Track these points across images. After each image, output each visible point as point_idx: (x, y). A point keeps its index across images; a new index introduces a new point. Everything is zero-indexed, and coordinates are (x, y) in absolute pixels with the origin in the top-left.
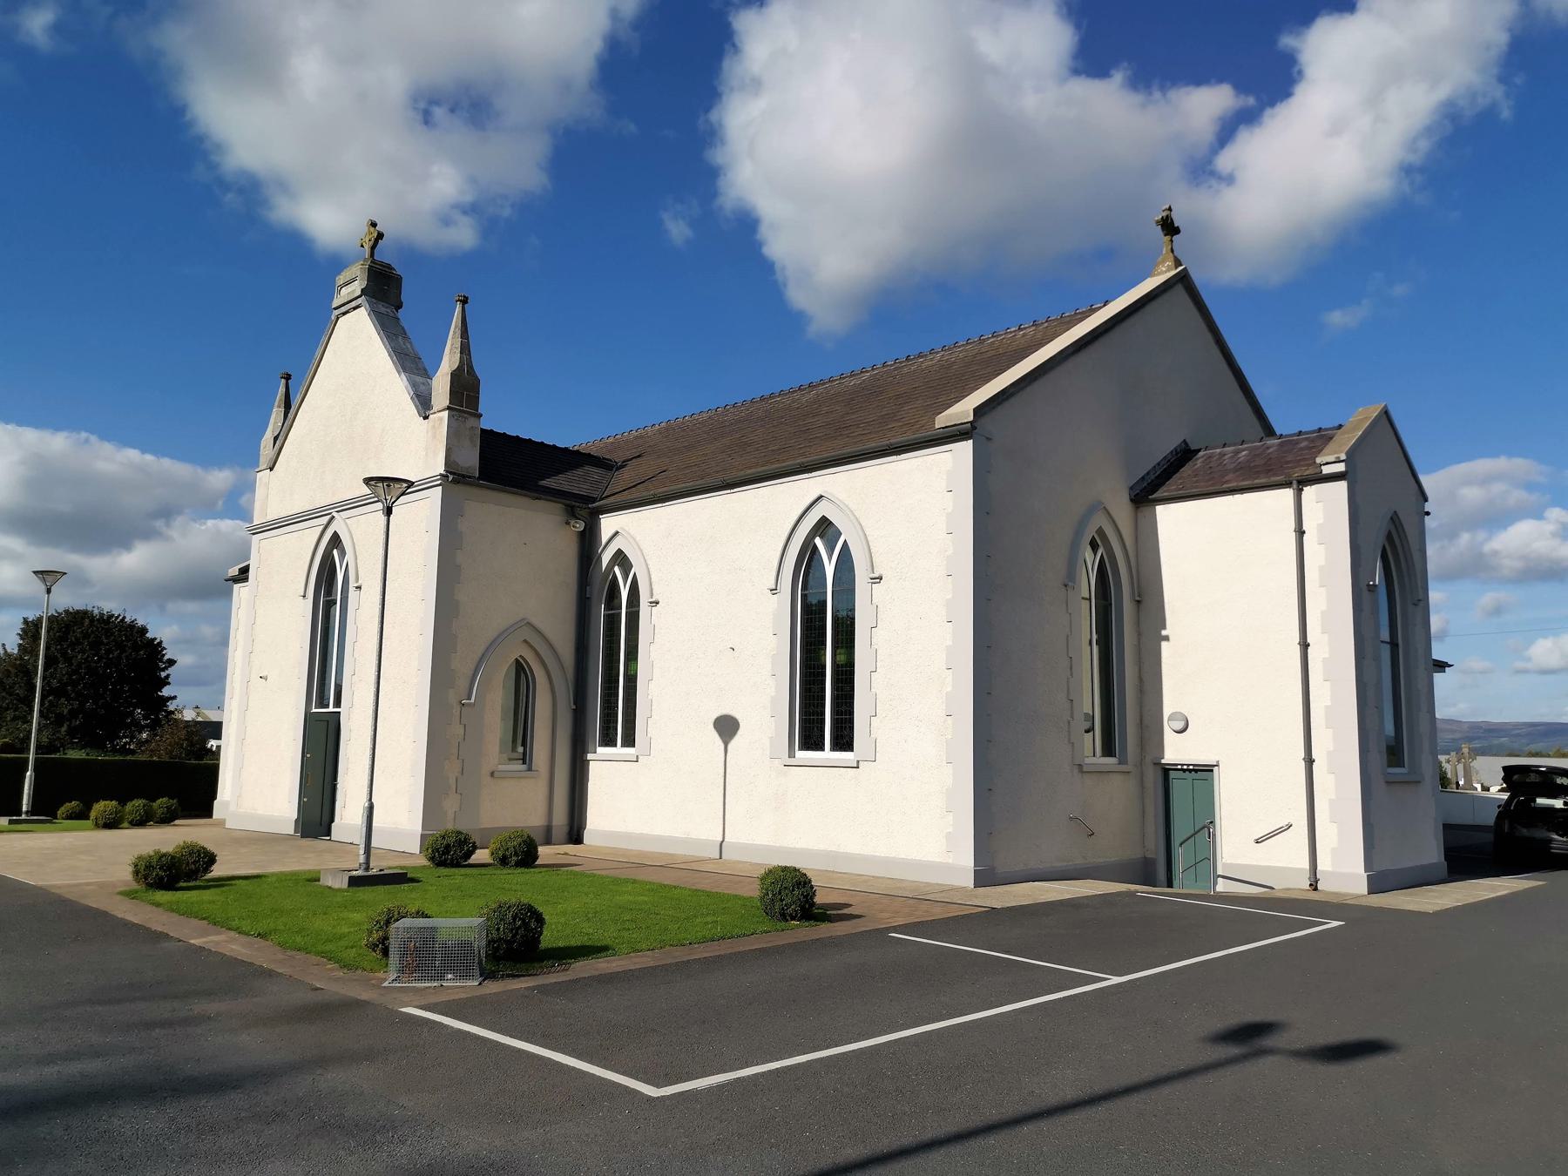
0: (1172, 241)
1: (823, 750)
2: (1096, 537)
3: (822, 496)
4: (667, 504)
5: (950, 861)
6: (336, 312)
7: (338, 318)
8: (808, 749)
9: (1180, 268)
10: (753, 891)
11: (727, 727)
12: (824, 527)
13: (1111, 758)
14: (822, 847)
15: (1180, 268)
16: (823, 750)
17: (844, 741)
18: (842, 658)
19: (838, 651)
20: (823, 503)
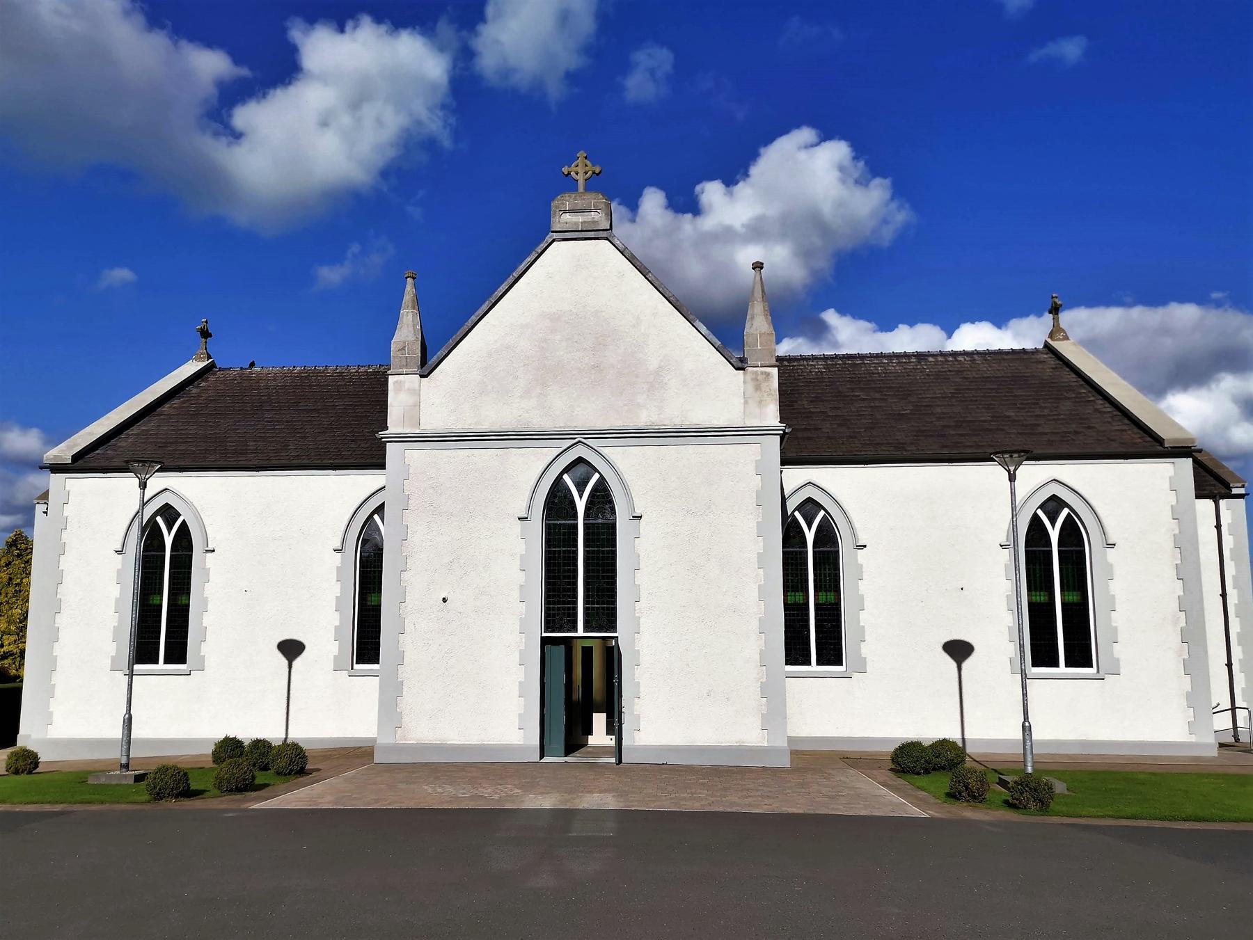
0: (206, 342)
1: (158, 663)
2: (1040, 513)
3: (166, 489)
4: (869, 465)
5: (1194, 740)
6: (555, 236)
7: (554, 241)
8: (791, 664)
9: (211, 360)
10: (209, 750)
11: (959, 650)
12: (169, 513)
13: (376, 665)
14: (1074, 739)
15: (211, 360)
16: (158, 663)
17: (177, 653)
18: (1074, 597)
19: (789, 594)
20: (167, 493)
